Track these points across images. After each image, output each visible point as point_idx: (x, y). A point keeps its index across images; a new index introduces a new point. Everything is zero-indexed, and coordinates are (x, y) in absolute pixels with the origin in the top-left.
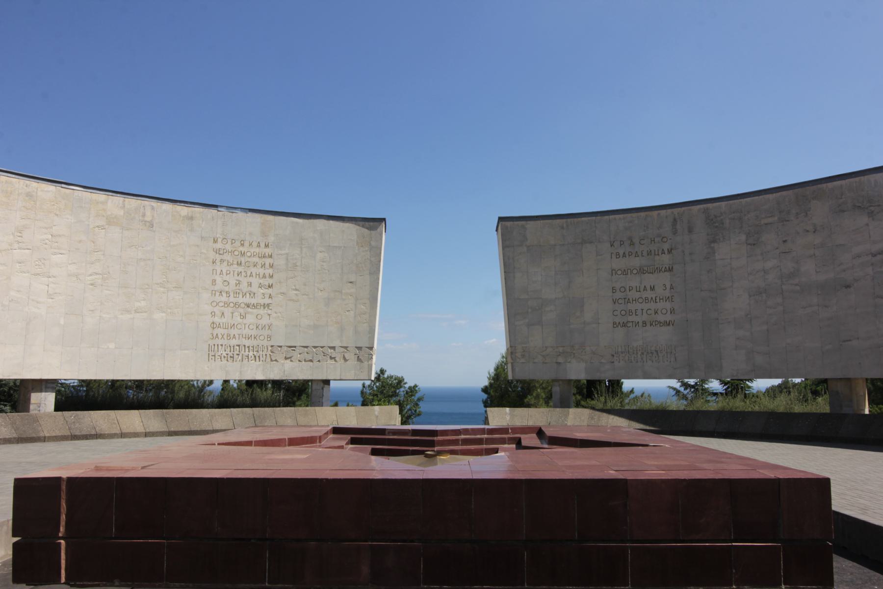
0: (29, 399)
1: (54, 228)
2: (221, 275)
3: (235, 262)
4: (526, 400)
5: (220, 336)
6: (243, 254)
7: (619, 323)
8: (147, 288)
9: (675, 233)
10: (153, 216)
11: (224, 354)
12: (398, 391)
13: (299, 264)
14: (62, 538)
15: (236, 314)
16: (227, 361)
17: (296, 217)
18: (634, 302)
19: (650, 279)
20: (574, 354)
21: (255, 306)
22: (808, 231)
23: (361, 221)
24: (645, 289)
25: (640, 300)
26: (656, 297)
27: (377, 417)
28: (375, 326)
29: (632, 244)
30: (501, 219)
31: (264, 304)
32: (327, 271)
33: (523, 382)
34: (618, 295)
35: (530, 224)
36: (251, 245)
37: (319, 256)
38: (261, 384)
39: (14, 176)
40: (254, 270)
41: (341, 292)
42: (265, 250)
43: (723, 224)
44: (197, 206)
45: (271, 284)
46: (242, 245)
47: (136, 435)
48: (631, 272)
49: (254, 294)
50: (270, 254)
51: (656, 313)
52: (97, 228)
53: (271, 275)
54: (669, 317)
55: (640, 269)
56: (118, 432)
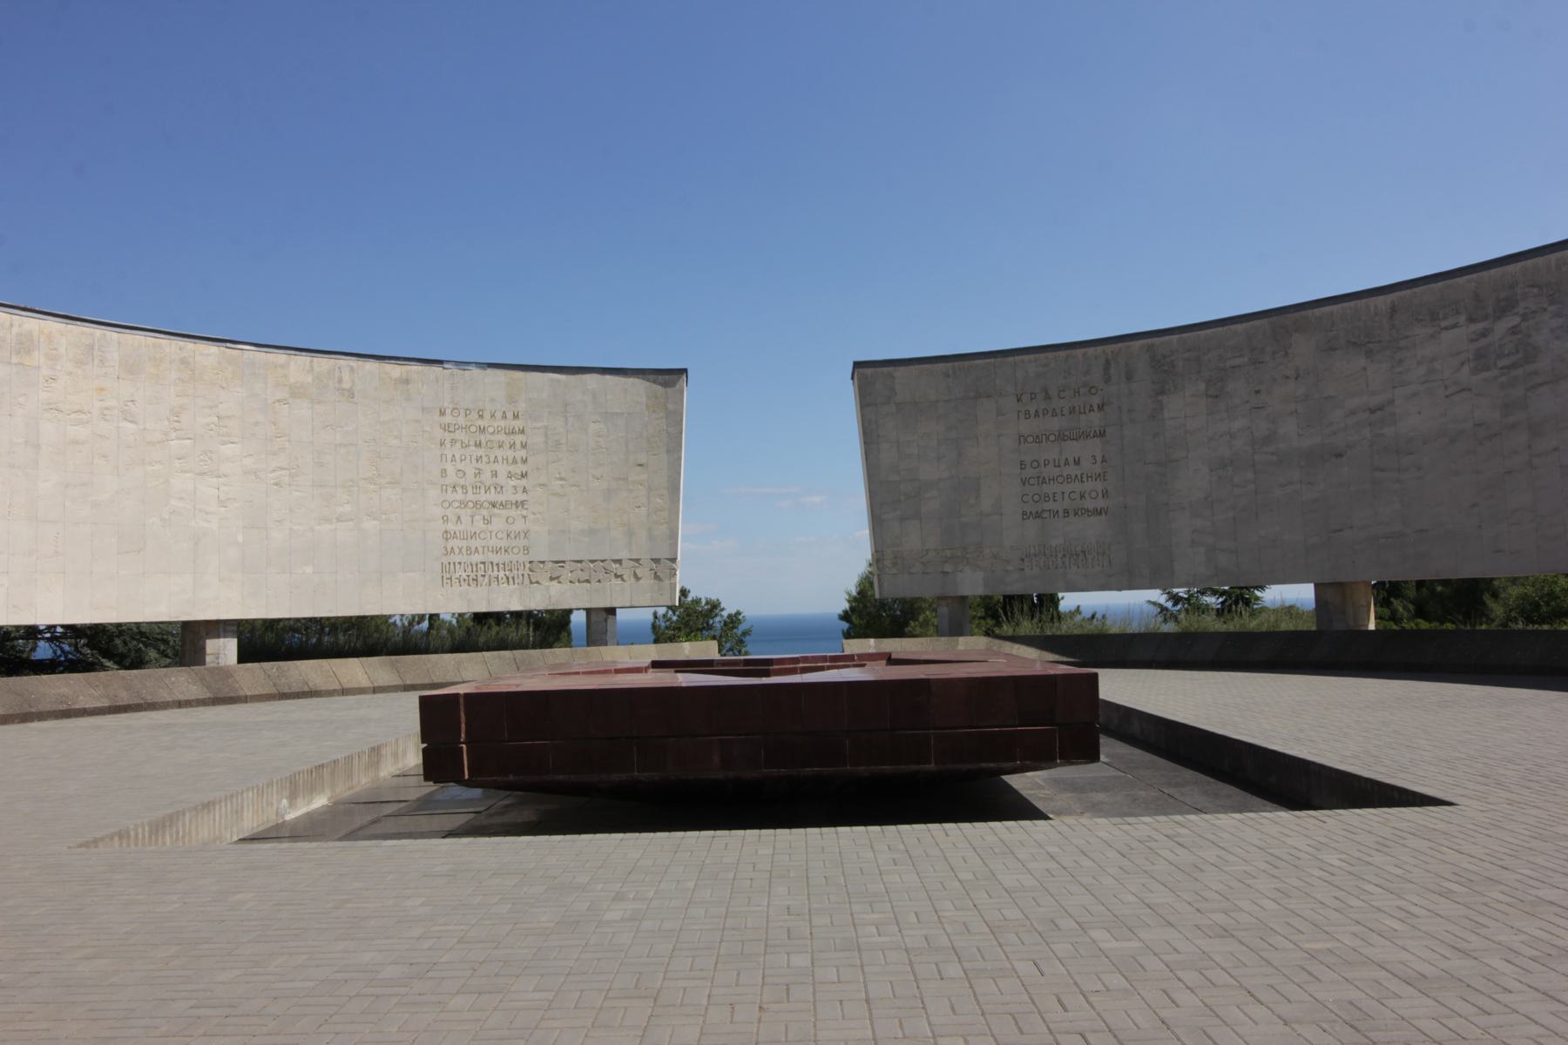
0: (203, 649)
1: (220, 406)
2: (453, 463)
3: (472, 443)
4: (906, 630)
5: (457, 551)
6: (482, 430)
8: (351, 486)
9: (1107, 380)
10: (353, 381)
11: (464, 575)
12: (711, 622)
13: (563, 441)
14: (463, 743)
15: (476, 517)
16: (469, 585)
17: (557, 373)
18: (1051, 482)
19: (1073, 449)
20: (967, 558)
21: (503, 505)
22: (1287, 377)
23: (650, 374)
24: (1067, 463)
25: (1060, 480)
26: (1082, 474)
28: (678, 529)
29: (1048, 397)
30: (857, 365)
33: (903, 601)
34: (1030, 472)
35: (900, 371)
36: (493, 416)
37: (593, 427)
38: (498, 617)
39: (162, 336)
40: (500, 453)
41: (626, 480)
43: (1174, 367)
44: (414, 363)
45: (524, 473)
46: (481, 417)
47: (361, 691)
48: (1047, 438)
49: (502, 487)
50: (521, 428)
51: (1082, 497)
52: (278, 403)
53: (524, 458)
54: (1101, 503)
55: (1059, 434)
56: (337, 687)
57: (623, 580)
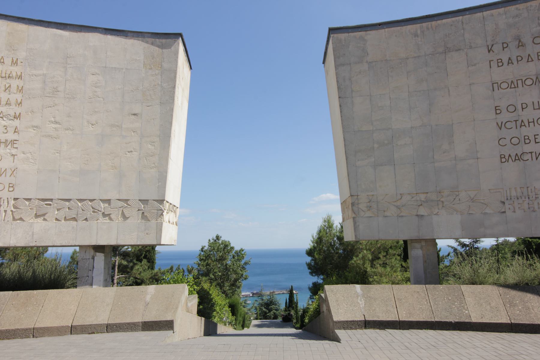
7: (510, 155)
18: (532, 124)
27: (147, 304)
29: (521, 45)
30: (332, 30)
31: (7, 140)
32: (102, 99)
34: (505, 116)
35: (372, 34)
42: (12, 68)
48: (524, 83)
50: (19, 74)
57: (111, 219)
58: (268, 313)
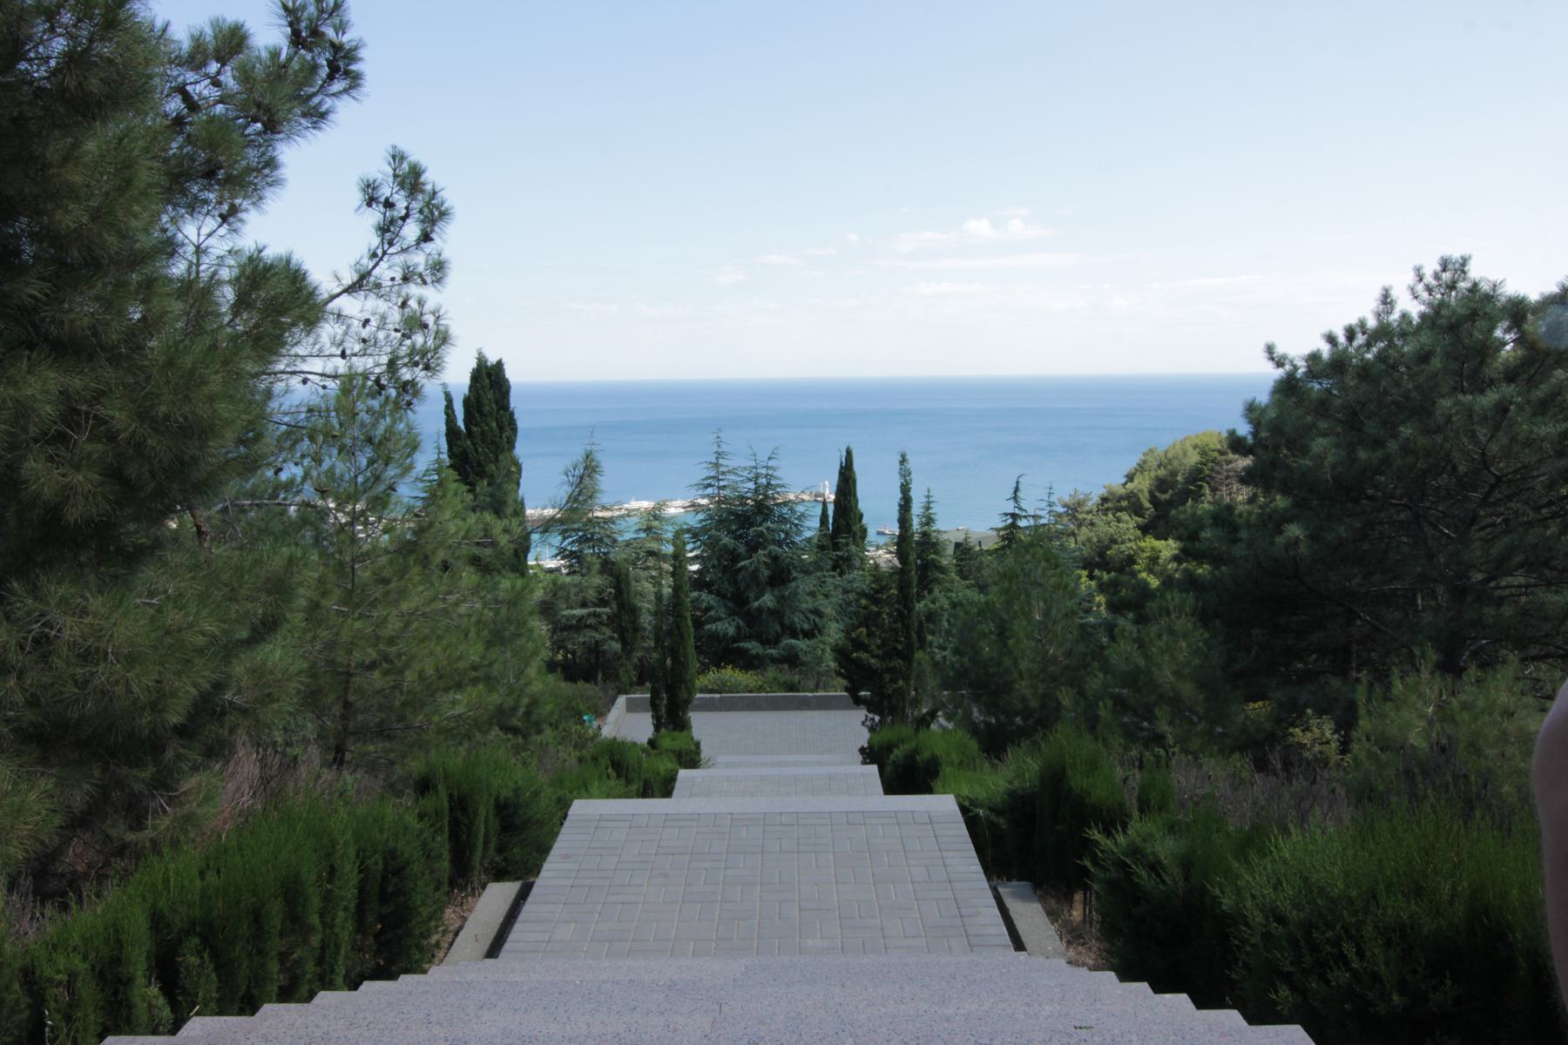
58: (744, 559)
